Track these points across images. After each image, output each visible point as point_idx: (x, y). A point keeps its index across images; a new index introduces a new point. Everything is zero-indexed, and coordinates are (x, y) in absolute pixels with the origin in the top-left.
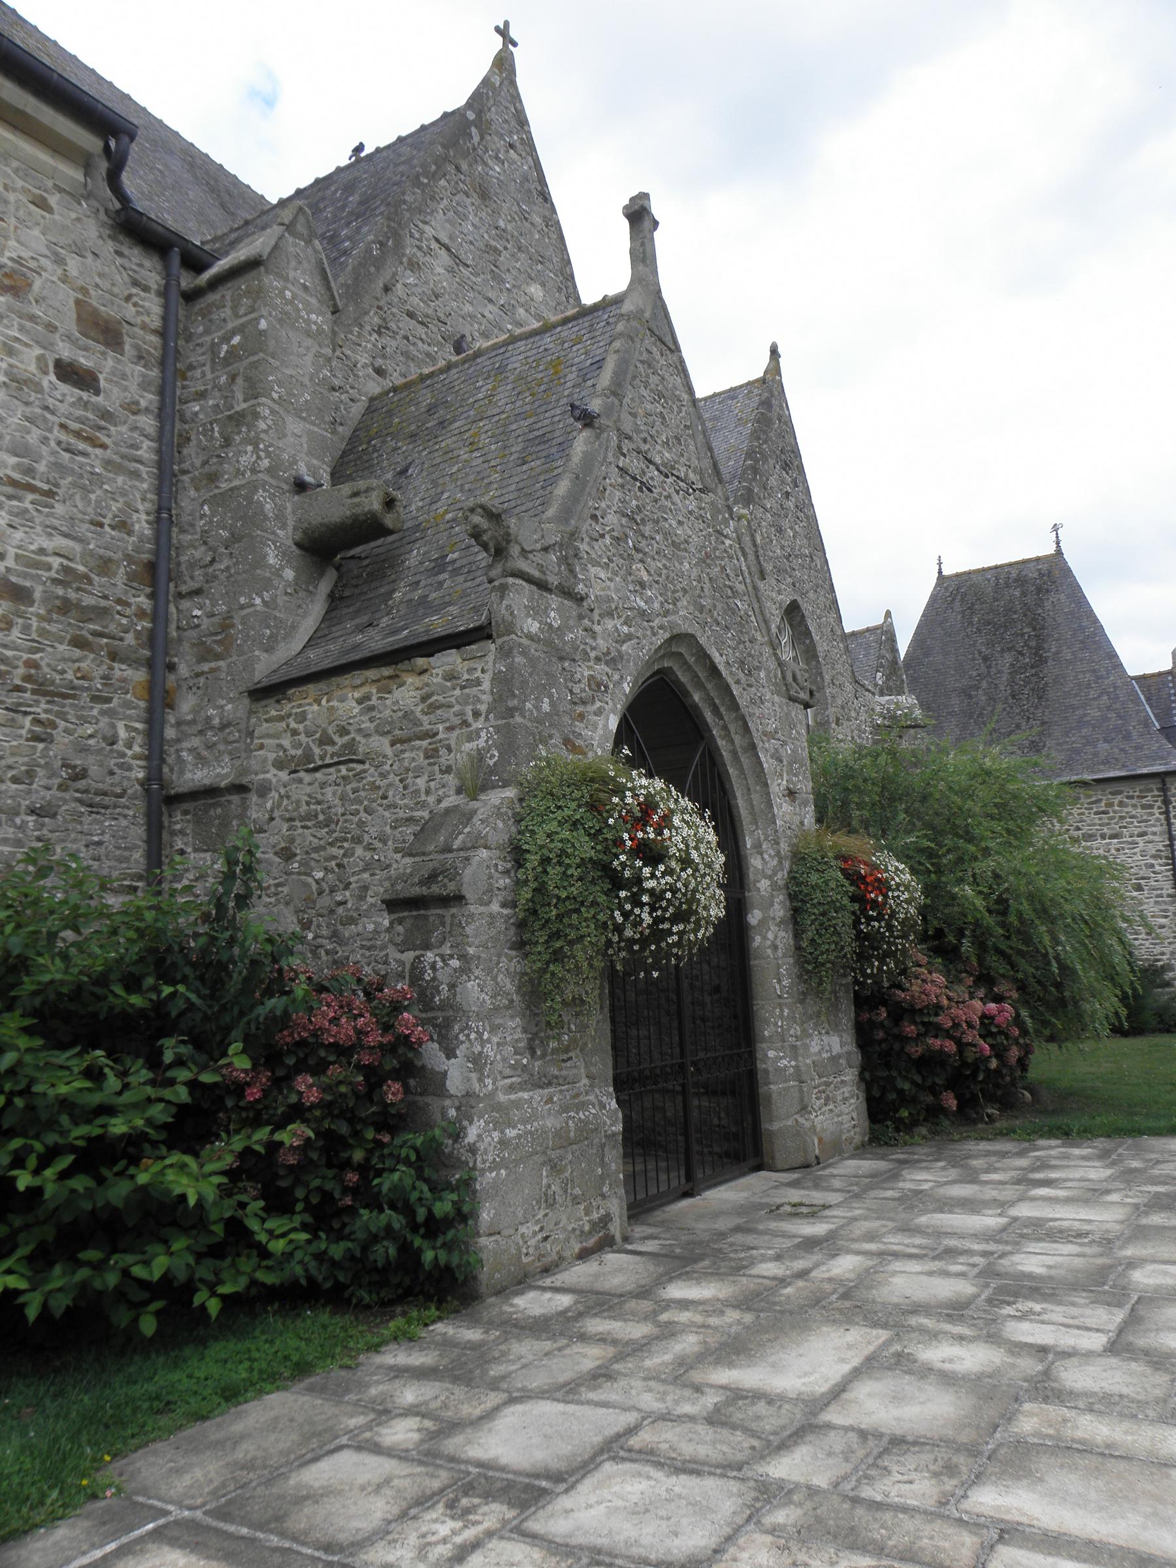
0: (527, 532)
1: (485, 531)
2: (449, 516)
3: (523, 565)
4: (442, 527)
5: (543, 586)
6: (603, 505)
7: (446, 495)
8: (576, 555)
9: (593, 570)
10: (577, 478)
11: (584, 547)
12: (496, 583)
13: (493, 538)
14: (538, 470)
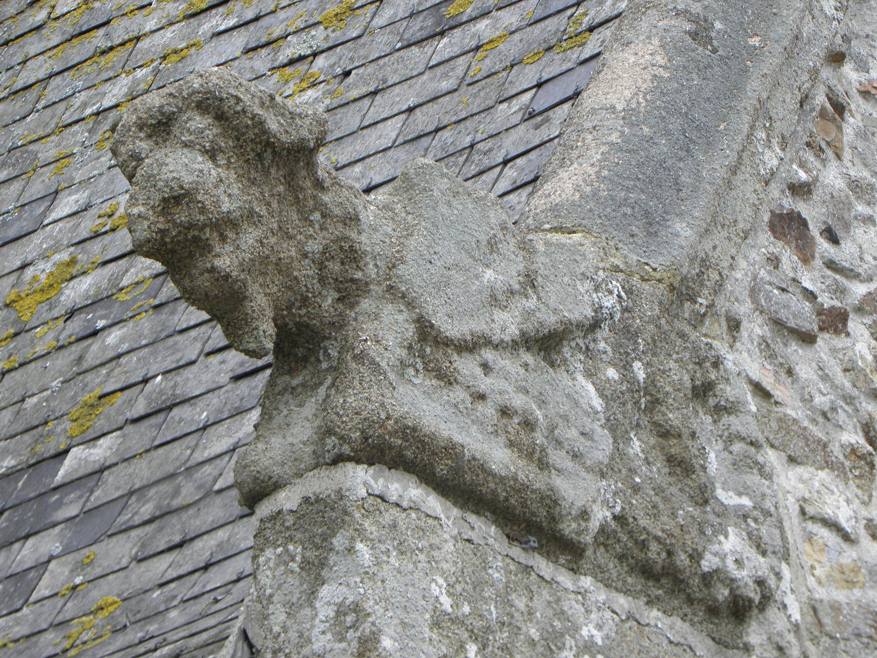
0: (442, 247)
1: (226, 225)
2: (76, 292)
3: (427, 407)
4: (44, 339)
5: (532, 524)
6: (832, 177)
7: (67, 204)
8: (702, 391)
9: (792, 482)
10: (700, 33)
11: (744, 360)
12: (287, 500)
13: (262, 264)
14: (511, 48)
